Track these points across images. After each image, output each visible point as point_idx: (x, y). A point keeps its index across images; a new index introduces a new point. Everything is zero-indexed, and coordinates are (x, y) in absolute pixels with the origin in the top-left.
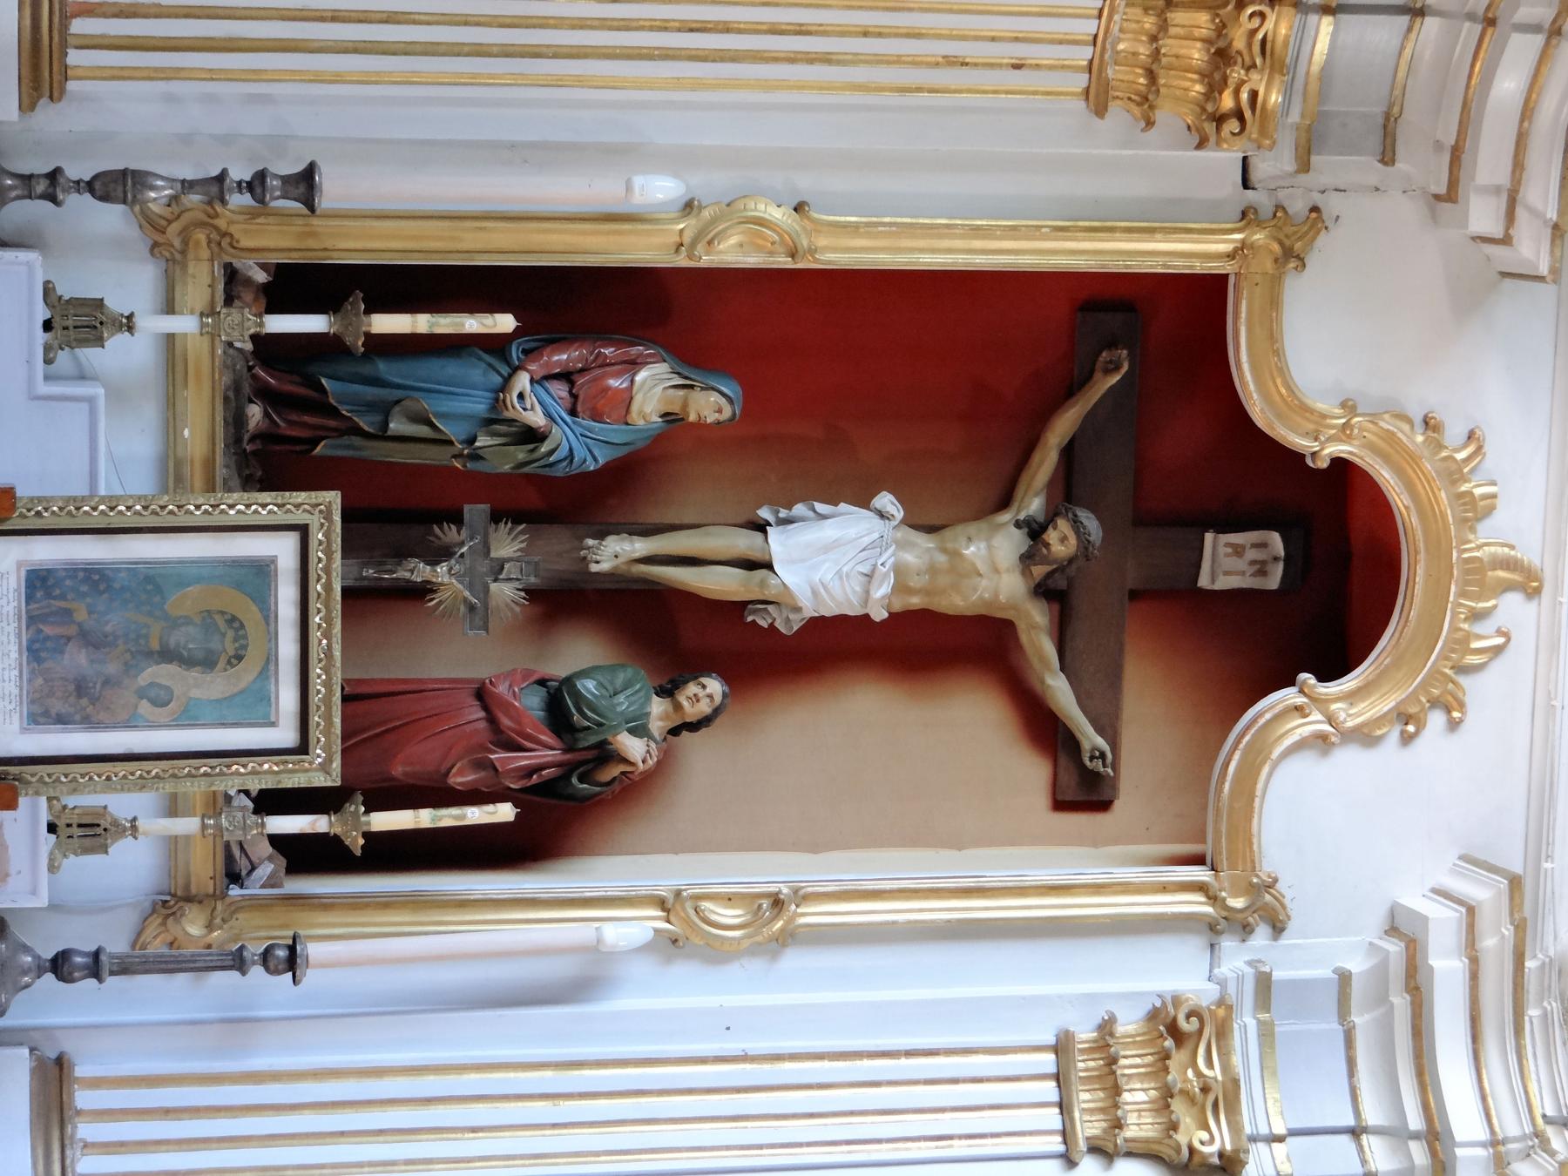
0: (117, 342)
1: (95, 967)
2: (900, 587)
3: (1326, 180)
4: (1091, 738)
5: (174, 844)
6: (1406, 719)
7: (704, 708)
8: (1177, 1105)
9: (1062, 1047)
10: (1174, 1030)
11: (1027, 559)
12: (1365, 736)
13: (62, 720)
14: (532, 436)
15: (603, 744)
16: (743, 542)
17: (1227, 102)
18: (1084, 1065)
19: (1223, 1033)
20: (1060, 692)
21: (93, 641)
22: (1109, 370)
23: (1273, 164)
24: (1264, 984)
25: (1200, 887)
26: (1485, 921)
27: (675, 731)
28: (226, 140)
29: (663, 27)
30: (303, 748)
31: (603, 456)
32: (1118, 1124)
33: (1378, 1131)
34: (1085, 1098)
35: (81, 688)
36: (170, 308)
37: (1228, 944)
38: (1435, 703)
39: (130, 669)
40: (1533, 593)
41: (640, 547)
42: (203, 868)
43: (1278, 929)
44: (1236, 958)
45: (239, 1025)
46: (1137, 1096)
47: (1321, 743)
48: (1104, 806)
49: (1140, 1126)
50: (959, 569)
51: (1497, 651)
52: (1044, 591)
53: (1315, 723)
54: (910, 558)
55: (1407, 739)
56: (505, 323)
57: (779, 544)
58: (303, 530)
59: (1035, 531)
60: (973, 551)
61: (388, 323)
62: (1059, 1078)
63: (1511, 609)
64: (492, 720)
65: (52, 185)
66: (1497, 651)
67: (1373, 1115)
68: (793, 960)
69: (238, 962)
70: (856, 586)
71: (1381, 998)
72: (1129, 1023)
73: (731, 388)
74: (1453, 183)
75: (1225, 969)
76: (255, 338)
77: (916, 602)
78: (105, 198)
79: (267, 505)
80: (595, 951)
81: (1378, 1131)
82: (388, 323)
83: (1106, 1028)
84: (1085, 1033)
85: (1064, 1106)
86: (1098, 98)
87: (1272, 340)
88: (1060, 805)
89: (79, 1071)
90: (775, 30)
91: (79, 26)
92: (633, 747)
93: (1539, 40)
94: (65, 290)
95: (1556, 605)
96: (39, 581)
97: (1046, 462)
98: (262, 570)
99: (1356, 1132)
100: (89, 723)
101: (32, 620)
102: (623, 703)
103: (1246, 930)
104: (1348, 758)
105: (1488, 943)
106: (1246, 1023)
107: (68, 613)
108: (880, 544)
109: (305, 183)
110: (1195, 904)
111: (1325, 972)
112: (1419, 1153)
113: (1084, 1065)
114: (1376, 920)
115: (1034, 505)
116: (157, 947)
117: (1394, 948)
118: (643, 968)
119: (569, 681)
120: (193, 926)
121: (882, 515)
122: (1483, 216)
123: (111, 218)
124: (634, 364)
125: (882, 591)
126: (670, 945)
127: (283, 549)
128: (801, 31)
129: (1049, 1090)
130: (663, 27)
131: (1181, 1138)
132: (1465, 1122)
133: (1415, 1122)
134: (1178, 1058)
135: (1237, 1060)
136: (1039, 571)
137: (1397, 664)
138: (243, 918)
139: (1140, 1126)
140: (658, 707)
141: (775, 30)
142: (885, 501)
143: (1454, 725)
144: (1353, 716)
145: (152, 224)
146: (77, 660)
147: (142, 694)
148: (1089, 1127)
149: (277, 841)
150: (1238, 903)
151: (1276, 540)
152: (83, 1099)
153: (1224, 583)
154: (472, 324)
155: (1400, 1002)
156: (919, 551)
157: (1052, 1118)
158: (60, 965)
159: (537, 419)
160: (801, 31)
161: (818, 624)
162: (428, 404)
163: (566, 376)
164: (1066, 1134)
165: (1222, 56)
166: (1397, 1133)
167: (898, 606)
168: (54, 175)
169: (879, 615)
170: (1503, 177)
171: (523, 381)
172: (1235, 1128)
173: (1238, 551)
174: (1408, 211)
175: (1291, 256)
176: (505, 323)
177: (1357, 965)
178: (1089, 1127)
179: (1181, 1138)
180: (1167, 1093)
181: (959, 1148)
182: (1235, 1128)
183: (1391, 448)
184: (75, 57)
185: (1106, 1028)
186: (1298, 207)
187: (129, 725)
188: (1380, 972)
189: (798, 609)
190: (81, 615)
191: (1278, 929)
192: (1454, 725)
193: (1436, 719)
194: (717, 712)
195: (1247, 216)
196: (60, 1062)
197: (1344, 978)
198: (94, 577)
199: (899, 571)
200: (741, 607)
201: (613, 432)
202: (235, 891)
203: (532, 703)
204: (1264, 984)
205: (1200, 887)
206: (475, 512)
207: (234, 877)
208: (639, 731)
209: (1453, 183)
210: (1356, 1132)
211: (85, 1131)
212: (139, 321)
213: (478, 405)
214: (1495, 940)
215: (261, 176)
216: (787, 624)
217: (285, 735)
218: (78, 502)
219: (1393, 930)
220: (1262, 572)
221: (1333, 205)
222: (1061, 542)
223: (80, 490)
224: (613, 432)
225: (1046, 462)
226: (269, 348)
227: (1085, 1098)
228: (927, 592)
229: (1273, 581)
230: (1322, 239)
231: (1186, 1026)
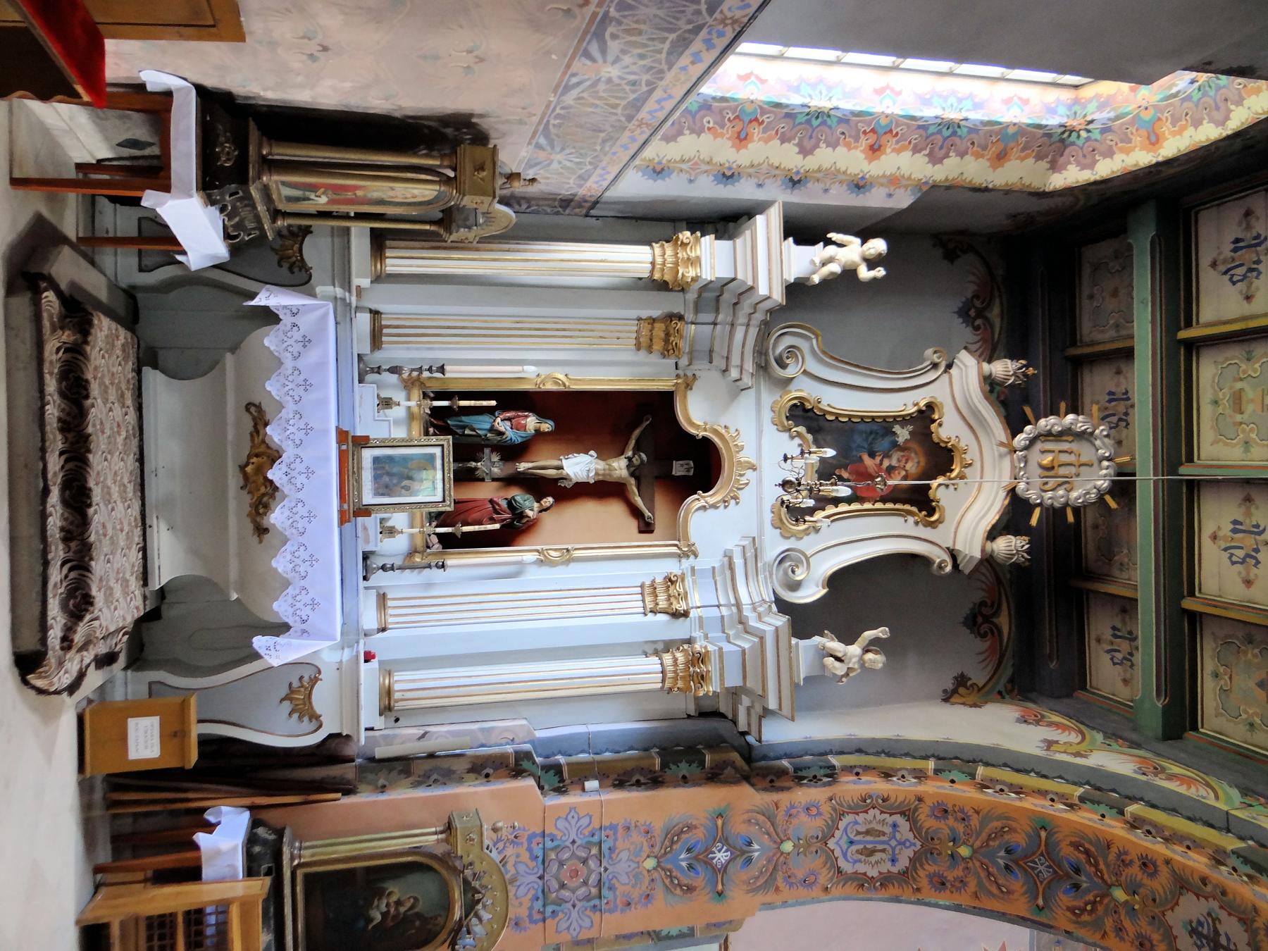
0: (395, 408)
1: (392, 568)
2: (597, 474)
3: (696, 367)
4: (647, 513)
5: (412, 536)
6: (725, 502)
7: (548, 504)
8: (672, 599)
9: (642, 586)
10: (670, 580)
11: (628, 467)
12: (714, 506)
13: (383, 495)
14: (501, 434)
15: (522, 512)
16: (555, 463)
17: (670, 347)
18: (647, 591)
19: (683, 580)
20: (639, 501)
21: (390, 474)
22: (647, 420)
23: (684, 361)
24: (693, 569)
25: (676, 545)
26: (747, 550)
27: (540, 511)
28: (422, 359)
29: (530, 329)
30: (444, 501)
31: (520, 440)
32: (657, 604)
33: (724, 606)
34: (648, 599)
35: (387, 487)
36: (409, 399)
37: (684, 560)
38: (732, 498)
39: (399, 482)
40: (755, 470)
41: (530, 465)
42: (419, 542)
43: (696, 556)
44: (686, 564)
45: (429, 585)
46: (662, 598)
47: (704, 508)
48: (652, 532)
49: (663, 604)
50: (611, 469)
51: (747, 484)
52: (632, 475)
53: (702, 503)
54: (599, 467)
55: (726, 507)
56: (493, 403)
57: (565, 463)
58: (442, 446)
59: (630, 459)
60: (615, 465)
61: (463, 403)
62: (642, 594)
63: (750, 474)
64: (494, 507)
65: (378, 370)
66: (747, 484)
67: (722, 602)
68: (572, 565)
69: (429, 566)
70: (585, 474)
71: (723, 573)
72: (659, 580)
73: (552, 423)
74: (727, 366)
75: (683, 567)
76: (431, 409)
77: (601, 478)
78: (392, 373)
79: (434, 440)
80: (520, 563)
81: (724, 606)
82: (463, 403)
83: (653, 581)
84: (648, 583)
85: (643, 601)
86: (638, 347)
87: (685, 409)
88: (641, 532)
89: (389, 596)
90: (558, 330)
91: (385, 331)
92: (530, 513)
93: (744, 328)
94: (383, 396)
95: (761, 471)
96: (372, 229)
97: (632, 443)
98: (433, 456)
99: (718, 606)
100: (389, 495)
101: (375, 469)
102: (527, 503)
103: (688, 557)
104: (711, 512)
105: (748, 555)
106: (689, 580)
107: (383, 468)
108: (591, 463)
109: (442, 369)
110: (674, 549)
111: (709, 567)
112: (734, 609)
113: (647, 591)
114: (722, 553)
115: (630, 454)
116: (407, 563)
117: (726, 559)
118: (534, 568)
119: (513, 498)
120: (418, 559)
121: (591, 456)
122: (734, 373)
123: (393, 378)
124: (527, 417)
125: (592, 474)
126: (540, 563)
127: (437, 451)
128: (564, 330)
129: (639, 597)
130: (530, 329)
131: (673, 607)
132: (745, 599)
133: (733, 601)
134: (672, 588)
135: (687, 587)
136: (632, 469)
137: (721, 488)
138: (430, 557)
139: (663, 604)
140: (536, 505)
141: (558, 330)
142: (592, 452)
143: (737, 503)
144: (711, 500)
145: (404, 380)
146: (386, 479)
147: (403, 488)
148: (650, 605)
149: (439, 535)
150: (686, 549)
151: (691, 463)
152: (390, 603)
153: (679, 474)
154: (485, 403)
155: (728, 573)
156: (601, 465)
157: (641, 604)
158: (383, 568)
159: (502, 429)
160: (564, 330)
161: (577, 484)
162: (475, 426)
163: (509, 419)
164: (644, 607)
165: (668, 335)
166: (728, 605)
167: (597, 479)
168: (379, 367)
169: (592, 481)
170: (739, 363)
171: (499, 420)
172: (687, 604)
173: (682, 465)
174: (716, 375)
175: (688, 386)
176: (493, 403)
177: (717, 565)
178: (650, 605)
179: (673, 607)
180: (669, 596)
181: (559, 346)
182: (687, 604)
183: (716, 432)
184: (384, 339)
185: (653, 581)
186: (690, 374)
187: (399, 496)
188: (722, 566)
189: (571, 480)
190: (387, 468)
191: (696, 556)
192: (737, 503)
193: (733, 502)
194: (551, 506)
195: (678, 376)
196: (384, 594)
197: (714, 568)
198: (390, 459)
199: (596, 470)
200: (557, 480)
201: (522, 433)
202: (428, 550)
203: (504, 504)
204: (693, 569)
205: (676, 545)
206: (487, 451)
207: (428, 547)
208: (532, 510)
209: (727, 366)
210: (718, 606)
211: (390, 611)
212: (401, 403)
213: (488, 426)
214: (750, 554)
215: (431, 367)
216: (568, 485)
217: (437, 451)
218: (386, 439)
219: (725, 556)
220: (688, 471)
221: (697, 373)
222: (636, 461)
223: (387, 436)
224: (522, 433)
225: (632, 443)
226: (434, 409)
227: (648, 599)
228: (604, 475)
229: (691, 473)
230: (697, 382)
231: (673, 579)
